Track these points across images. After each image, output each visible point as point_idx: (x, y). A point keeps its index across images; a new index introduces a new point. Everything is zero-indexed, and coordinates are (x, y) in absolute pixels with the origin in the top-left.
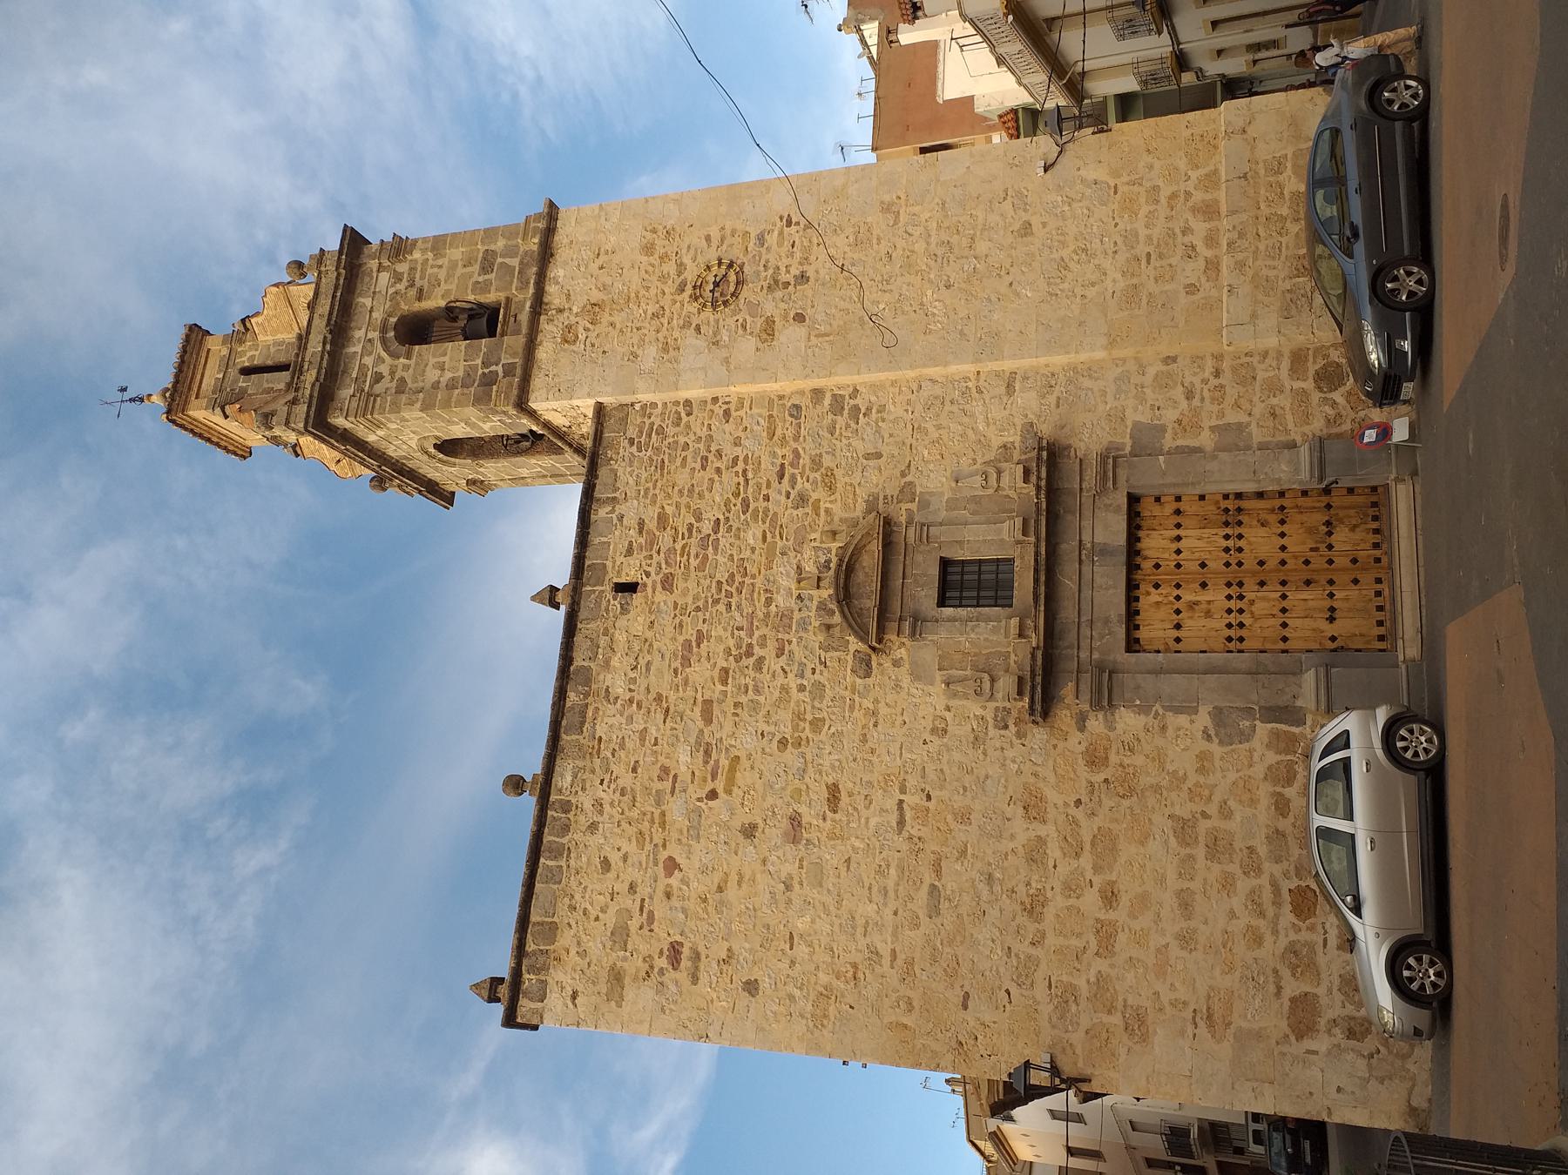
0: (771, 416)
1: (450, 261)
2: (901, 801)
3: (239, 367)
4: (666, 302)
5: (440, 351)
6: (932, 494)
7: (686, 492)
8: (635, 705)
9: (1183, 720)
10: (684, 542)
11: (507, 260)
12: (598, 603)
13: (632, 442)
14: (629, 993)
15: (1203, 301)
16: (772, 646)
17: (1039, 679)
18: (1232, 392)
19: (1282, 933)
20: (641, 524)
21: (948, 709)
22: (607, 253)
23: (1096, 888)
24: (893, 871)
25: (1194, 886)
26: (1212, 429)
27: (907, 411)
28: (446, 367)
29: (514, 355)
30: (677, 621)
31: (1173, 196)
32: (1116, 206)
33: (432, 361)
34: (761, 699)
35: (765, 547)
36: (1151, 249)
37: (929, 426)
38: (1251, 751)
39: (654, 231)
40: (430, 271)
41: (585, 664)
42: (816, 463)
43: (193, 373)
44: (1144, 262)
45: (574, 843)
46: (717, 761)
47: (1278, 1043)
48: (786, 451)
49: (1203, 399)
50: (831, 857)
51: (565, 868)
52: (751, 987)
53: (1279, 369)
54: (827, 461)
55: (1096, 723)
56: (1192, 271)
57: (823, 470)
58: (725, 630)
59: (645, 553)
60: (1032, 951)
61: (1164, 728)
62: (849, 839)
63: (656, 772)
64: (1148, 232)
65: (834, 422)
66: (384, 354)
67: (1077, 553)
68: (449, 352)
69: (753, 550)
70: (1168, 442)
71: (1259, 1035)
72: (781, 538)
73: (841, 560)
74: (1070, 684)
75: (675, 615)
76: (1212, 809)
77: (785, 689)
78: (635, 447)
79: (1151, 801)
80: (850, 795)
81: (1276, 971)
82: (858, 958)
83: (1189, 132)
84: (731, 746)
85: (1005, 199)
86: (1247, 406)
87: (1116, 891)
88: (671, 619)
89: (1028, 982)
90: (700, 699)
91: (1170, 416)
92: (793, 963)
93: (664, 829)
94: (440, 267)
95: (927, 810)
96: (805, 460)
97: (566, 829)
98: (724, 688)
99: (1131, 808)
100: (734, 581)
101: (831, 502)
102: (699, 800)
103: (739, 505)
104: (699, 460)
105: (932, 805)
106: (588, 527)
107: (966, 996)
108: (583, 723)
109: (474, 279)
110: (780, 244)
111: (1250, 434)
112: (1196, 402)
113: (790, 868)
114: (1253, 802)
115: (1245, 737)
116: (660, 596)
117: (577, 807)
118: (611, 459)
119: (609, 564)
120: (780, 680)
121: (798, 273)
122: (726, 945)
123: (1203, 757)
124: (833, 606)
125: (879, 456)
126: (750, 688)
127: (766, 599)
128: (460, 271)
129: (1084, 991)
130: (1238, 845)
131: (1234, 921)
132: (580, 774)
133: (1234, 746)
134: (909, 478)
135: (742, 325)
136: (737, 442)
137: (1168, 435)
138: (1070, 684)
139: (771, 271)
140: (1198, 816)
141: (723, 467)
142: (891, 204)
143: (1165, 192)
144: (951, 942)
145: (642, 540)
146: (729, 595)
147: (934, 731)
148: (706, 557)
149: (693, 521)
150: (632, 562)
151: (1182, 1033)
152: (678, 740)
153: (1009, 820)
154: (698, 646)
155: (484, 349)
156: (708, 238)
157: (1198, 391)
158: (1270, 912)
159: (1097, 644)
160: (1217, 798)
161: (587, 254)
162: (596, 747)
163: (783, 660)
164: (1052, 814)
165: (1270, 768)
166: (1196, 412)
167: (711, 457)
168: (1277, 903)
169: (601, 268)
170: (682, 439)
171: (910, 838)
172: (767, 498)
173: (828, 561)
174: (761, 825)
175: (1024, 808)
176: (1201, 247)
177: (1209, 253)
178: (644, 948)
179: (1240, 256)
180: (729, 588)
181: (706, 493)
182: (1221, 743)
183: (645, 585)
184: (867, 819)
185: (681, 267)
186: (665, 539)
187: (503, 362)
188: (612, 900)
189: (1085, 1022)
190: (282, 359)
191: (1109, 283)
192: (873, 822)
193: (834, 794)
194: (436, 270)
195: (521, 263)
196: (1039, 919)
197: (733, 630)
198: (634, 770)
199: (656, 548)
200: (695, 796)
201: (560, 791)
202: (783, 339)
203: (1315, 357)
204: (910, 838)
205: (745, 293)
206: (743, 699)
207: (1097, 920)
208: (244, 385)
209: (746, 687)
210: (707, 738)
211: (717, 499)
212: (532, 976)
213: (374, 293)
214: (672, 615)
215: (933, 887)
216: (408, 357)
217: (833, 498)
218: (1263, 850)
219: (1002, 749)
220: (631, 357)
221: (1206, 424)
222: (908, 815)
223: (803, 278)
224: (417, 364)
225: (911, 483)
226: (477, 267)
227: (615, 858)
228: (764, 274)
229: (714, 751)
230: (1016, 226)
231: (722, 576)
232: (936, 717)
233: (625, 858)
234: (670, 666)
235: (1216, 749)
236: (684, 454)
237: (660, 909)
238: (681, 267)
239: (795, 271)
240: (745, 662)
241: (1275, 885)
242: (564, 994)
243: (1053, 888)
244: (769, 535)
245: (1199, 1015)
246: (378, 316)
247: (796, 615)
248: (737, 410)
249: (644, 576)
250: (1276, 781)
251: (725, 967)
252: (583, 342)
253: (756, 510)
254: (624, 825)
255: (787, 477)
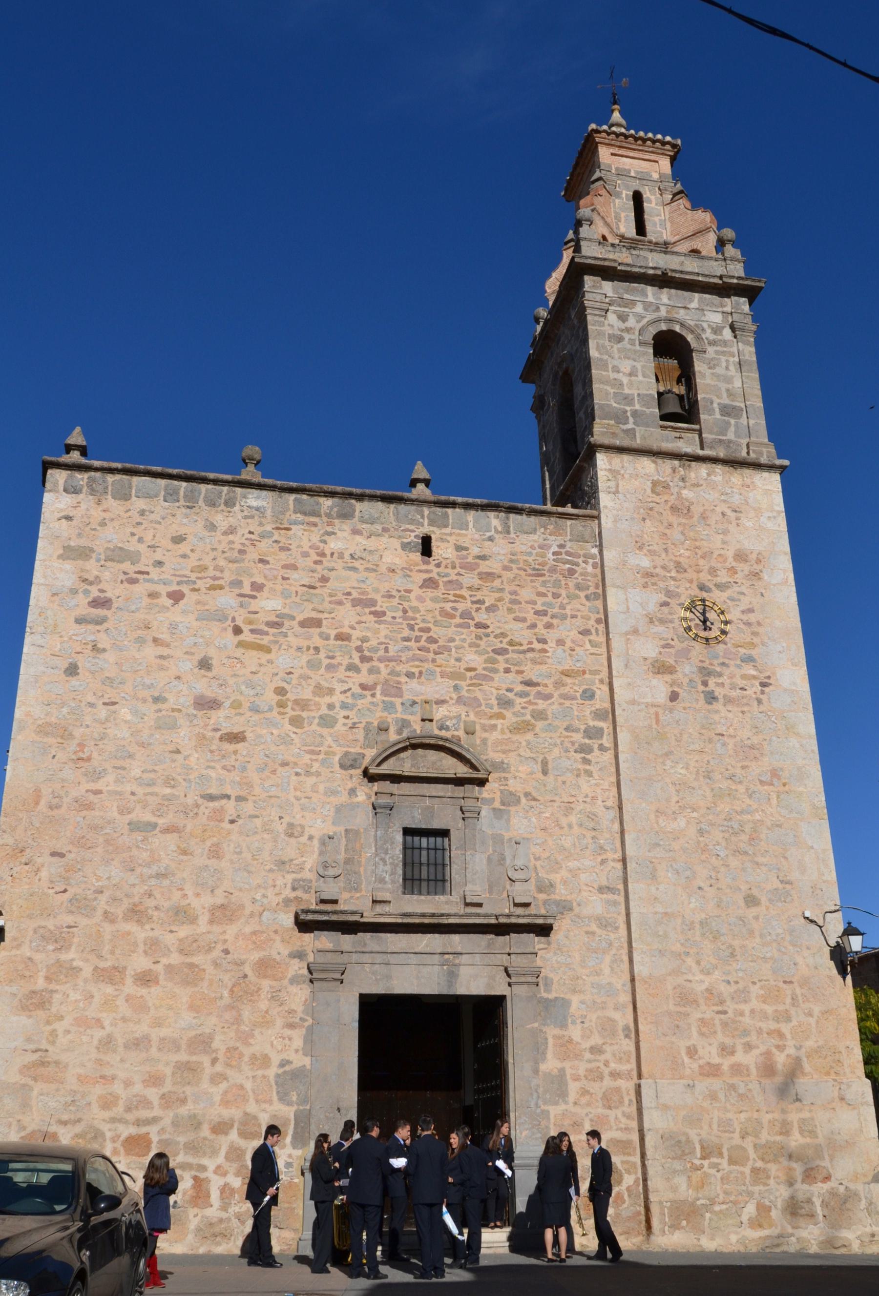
0: (584, 672)
1: (732, 377)
2: (228, 797)
3: (641, 190)
4: (691, 574)
5: (648, 372)
6: (508, 821)
7: (514, 597)
8: (319, 558)
9: (298, 1043)
10: (467, 597)
11: (732, 429)
12: (412, 522)
13: (561, 546)
14: (68, 566)
15: (680, 1061)
16: (369, 680)
17: (334, 918)
18: (598, 1089)
19: (113, 1126)
20: (483, 558)
21: (311, 838)
22: (738, 519)
23: (153, 967)
24: (168, 791)
25: (154, 1051)
26: (562, 1071)
27: (586, 796)
28: (633, 378)
29: (643, 438)
30: (394, 593)
31: (781, 1035)
32: (772, 983)
33: (639, 366)
34: (322, 671)
35: (462, 670)
36: (730, 1014)
37: (573, 819)
38: (270, 1102)
39: (759, 561)
40: (723, 359)
41: (357, 513)
42: (540, 715)
43: (634, 150)
44: (720, 1008)
45: (198, 511)
46: (267, 634)
47: (19, 1121)
48: (550, 689)
49: (589, 1061)
50: (184, 735)
51: (177, 504)
52: (72, 670)
53: (617, 1130)
54: (540, 725)
55: (298, 968)
56: (710, 1053)
57: (533, 721)
58: (386, 637)
59: (457, 562)
60: (99, 912)
61: (291, 1026)
62: (197, 751)
63: (260, 580)
64: (747, 1013)
65: (577, 730)
66: (645, 321)
67: (450, 951)
68: (647, 379)
69: (458, 660)
70: (551, 1032)
71: (25, 1105)
72: (470, 685)
73: (447, 740)
74: (332, 945)
75: (399, 591)
76: (219, 1068)
77: (331, 691)
78: (556, 549)
79: (228, 1016)
80: (235, 752)
81: (79, 1120)
82: (95, 763)
83: (843, 1050)
84: (280, 646)
85: (782, 882)
86: (584, 1100)
87: (150, 984)
88: (396, 587)
89: (73, 909)
90: (320, 616)
91: (575, 1032)
92: (91, 705)
93: (209, 589)
94: (727, 368)
95: (222, 821)
96: (542, 705)
97: (212, 504)
98: (332, 637)
99: (221, 997)
100: (431, 643)
101: (502, 729)
102: (234, 619)
103: (502, 646)
104: (545, 608)
105: (226, 825)
106: (482, 510)
107: (62, 855)
108: (305, 514)
109: (715, 399)
110: (744, 677)
111: (556, 1103)
112: (588, 1055)
113: (172, 701)
114: (225, 1103)
115: (283, 1098)
116: (420, 578)
117: (229, 512)
118: (546, 529)
119: (447, 530)
120: (339, 687)
121: (716, 694)
122: (108, 647)
123: (265, 1061)
124: (405, 735)
125: (545, 772)
126: (333, 661)
127: (413, 673)
128: (723, 386)
129: (64, 957)
130: (188, 1090)
131: (122, 1085)
132: (258, 513)
133: (275, 1087)
134: (523, 800)
135: (668, 644)
136: (560, 642)
137: (557, 1032)
138: (332, 945)
139: (718, 669)
140: (214, 1055)
141: (537, 630)
142: (779, 778)
143: (785, 1028)
144: (107, 841)
145: (470, 560)
146: (418, 639)
147: (291, 825)
148: (453, 617)
149: (487, 604)
150: (449, 551)
151: (29, 1040)
152: (286, 598)
153: (212, 891)
154: (371, 613)
155: (648, 411)
156: (751, 611)
157: (600, 1058)
158: (130, 1117)
159: (367, 968)
160: (229, 1072)
161: (736, 499)
162: (282, 526)
163: (357, 690)
164: (216, 929)
165: (255, 1118)
166: (578, 1056)
167: (546, 619)
168: (138, 1123)
169: (723, 514)
170: (564, 593)
171: (197, 806)
172: (507, 671)
173: (447, 729)
174: (210, 674)
175: (223, 905)
176: (733, 1060)
177: (725, 1067)
178: (106, 575)
179: (721, 1096)
180: (424, 638)
181: (513, 615)
182: (278, 1076)
183: (428, 563)
184: (213, 768)
185: (721, 587)
186: (470, 579)
187: (637, 429)
188: (149, 547)
189: (38, 957)
190: (649, 227)
191: (700, 977)
192: (213, 774)
193: (236, 738)
194: (724, 364)
195: (730, 441)
196: (126, 918)
197: (385, 643)
198: (261, 561)
199: (462, 571)
200: (236, 615)
201: (245, 497)
202: (655, 682)
203: (627, 1162)
204: (197, 806)
205: (698, 647)
206: (322, 655)
207: (125, 968)
208: (624, 196)
209: (332, 658)
210: (287, 623)
211: (507, 627)
212: (86, 480)
213: (703, 310)
214: (400, 589)
215: (154, 826)
216: (641, 343)
217: (507, 731)
218: (183, 1111)
219: (275, 886)
220: (639, 544)
221: (567, 1065)
222: (216, 804)
223: (711, 698)
224: (635, 351)
225: (518, 801)
226: (726, 401)
227: (184, 548)
228: (716, 662)
229: (276, 631)
230: (755, 892)
231: (436, 632)
232: (302, 827)
233: (184, 556)
234: (354, 588)
235: (272, 1072)
236: (550, 594)
237: (140, 589)
238: (721, 587)
239: (719, 692)
240: (356, 656)
241: (155, 1120)
242: (70, 509)
243: (152, 929)
244: (473, 673)
245: (43, 1054)
246: (681, 314)
247: (398, 701)
248: (590, 641)
249: (436, 562)
250: (244, 1123)
251: (90, 647)
252: (654, 499)
253: (494, 661)
254: (212, 555)
255: (528, 688)
